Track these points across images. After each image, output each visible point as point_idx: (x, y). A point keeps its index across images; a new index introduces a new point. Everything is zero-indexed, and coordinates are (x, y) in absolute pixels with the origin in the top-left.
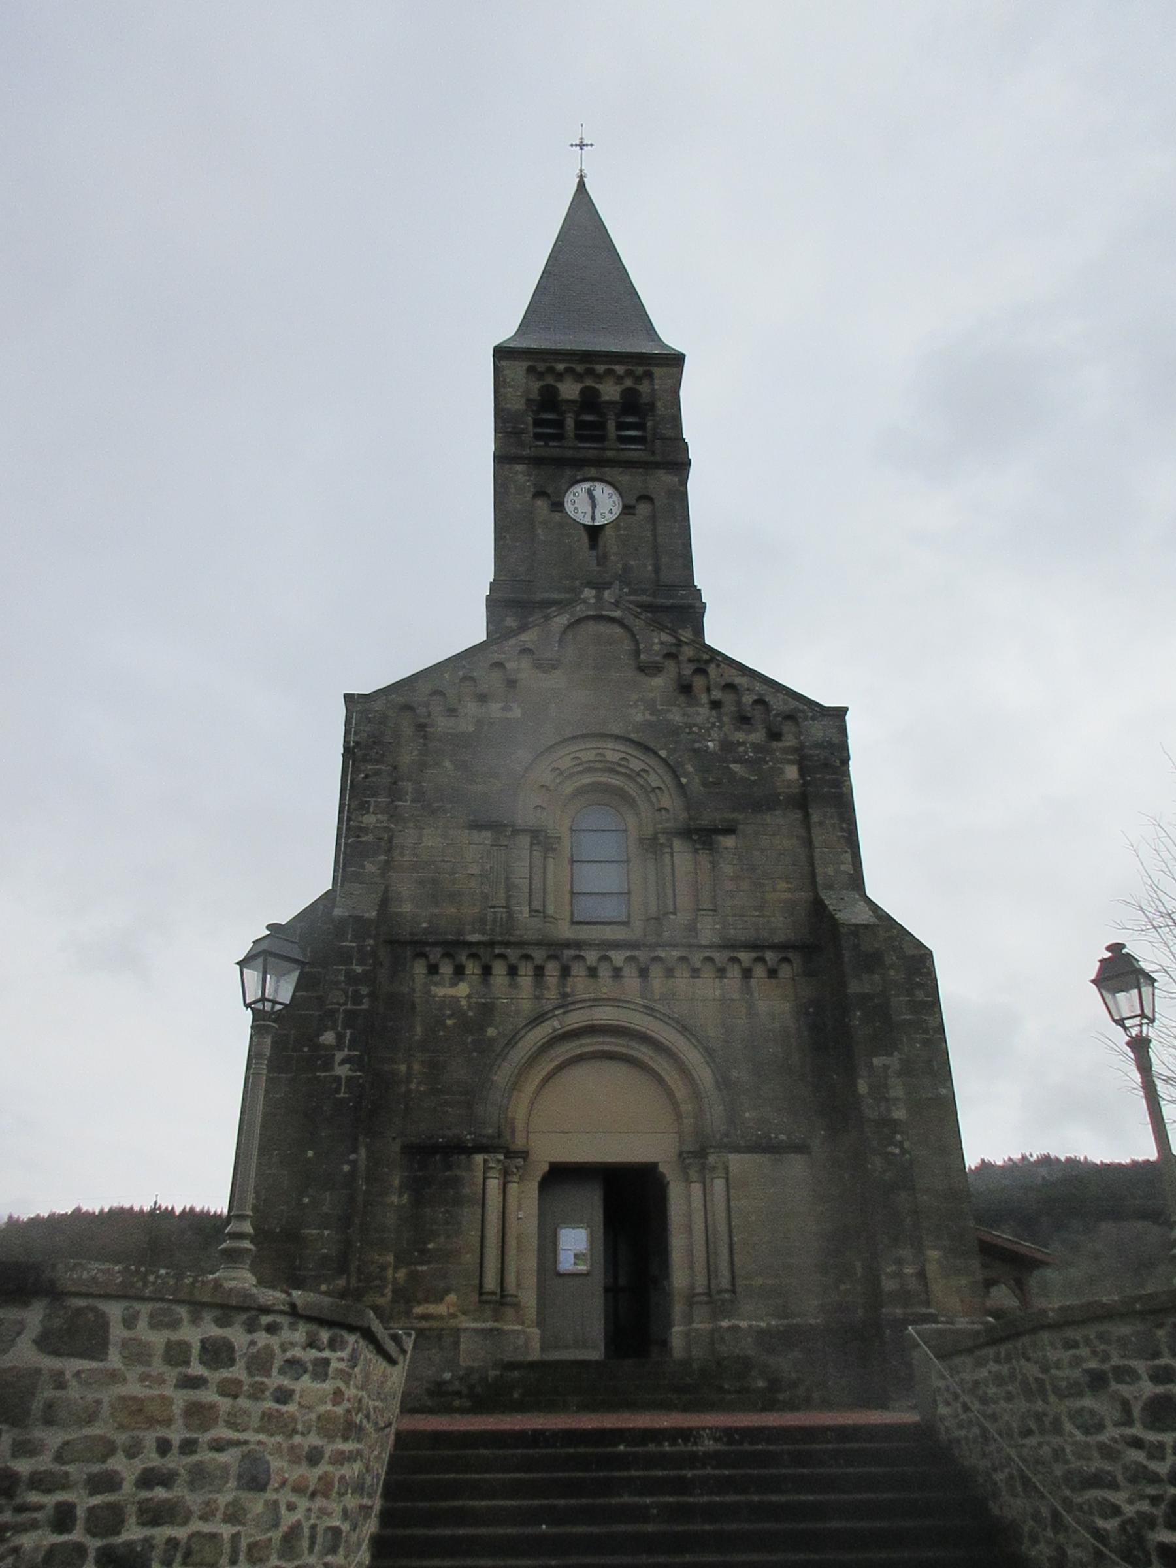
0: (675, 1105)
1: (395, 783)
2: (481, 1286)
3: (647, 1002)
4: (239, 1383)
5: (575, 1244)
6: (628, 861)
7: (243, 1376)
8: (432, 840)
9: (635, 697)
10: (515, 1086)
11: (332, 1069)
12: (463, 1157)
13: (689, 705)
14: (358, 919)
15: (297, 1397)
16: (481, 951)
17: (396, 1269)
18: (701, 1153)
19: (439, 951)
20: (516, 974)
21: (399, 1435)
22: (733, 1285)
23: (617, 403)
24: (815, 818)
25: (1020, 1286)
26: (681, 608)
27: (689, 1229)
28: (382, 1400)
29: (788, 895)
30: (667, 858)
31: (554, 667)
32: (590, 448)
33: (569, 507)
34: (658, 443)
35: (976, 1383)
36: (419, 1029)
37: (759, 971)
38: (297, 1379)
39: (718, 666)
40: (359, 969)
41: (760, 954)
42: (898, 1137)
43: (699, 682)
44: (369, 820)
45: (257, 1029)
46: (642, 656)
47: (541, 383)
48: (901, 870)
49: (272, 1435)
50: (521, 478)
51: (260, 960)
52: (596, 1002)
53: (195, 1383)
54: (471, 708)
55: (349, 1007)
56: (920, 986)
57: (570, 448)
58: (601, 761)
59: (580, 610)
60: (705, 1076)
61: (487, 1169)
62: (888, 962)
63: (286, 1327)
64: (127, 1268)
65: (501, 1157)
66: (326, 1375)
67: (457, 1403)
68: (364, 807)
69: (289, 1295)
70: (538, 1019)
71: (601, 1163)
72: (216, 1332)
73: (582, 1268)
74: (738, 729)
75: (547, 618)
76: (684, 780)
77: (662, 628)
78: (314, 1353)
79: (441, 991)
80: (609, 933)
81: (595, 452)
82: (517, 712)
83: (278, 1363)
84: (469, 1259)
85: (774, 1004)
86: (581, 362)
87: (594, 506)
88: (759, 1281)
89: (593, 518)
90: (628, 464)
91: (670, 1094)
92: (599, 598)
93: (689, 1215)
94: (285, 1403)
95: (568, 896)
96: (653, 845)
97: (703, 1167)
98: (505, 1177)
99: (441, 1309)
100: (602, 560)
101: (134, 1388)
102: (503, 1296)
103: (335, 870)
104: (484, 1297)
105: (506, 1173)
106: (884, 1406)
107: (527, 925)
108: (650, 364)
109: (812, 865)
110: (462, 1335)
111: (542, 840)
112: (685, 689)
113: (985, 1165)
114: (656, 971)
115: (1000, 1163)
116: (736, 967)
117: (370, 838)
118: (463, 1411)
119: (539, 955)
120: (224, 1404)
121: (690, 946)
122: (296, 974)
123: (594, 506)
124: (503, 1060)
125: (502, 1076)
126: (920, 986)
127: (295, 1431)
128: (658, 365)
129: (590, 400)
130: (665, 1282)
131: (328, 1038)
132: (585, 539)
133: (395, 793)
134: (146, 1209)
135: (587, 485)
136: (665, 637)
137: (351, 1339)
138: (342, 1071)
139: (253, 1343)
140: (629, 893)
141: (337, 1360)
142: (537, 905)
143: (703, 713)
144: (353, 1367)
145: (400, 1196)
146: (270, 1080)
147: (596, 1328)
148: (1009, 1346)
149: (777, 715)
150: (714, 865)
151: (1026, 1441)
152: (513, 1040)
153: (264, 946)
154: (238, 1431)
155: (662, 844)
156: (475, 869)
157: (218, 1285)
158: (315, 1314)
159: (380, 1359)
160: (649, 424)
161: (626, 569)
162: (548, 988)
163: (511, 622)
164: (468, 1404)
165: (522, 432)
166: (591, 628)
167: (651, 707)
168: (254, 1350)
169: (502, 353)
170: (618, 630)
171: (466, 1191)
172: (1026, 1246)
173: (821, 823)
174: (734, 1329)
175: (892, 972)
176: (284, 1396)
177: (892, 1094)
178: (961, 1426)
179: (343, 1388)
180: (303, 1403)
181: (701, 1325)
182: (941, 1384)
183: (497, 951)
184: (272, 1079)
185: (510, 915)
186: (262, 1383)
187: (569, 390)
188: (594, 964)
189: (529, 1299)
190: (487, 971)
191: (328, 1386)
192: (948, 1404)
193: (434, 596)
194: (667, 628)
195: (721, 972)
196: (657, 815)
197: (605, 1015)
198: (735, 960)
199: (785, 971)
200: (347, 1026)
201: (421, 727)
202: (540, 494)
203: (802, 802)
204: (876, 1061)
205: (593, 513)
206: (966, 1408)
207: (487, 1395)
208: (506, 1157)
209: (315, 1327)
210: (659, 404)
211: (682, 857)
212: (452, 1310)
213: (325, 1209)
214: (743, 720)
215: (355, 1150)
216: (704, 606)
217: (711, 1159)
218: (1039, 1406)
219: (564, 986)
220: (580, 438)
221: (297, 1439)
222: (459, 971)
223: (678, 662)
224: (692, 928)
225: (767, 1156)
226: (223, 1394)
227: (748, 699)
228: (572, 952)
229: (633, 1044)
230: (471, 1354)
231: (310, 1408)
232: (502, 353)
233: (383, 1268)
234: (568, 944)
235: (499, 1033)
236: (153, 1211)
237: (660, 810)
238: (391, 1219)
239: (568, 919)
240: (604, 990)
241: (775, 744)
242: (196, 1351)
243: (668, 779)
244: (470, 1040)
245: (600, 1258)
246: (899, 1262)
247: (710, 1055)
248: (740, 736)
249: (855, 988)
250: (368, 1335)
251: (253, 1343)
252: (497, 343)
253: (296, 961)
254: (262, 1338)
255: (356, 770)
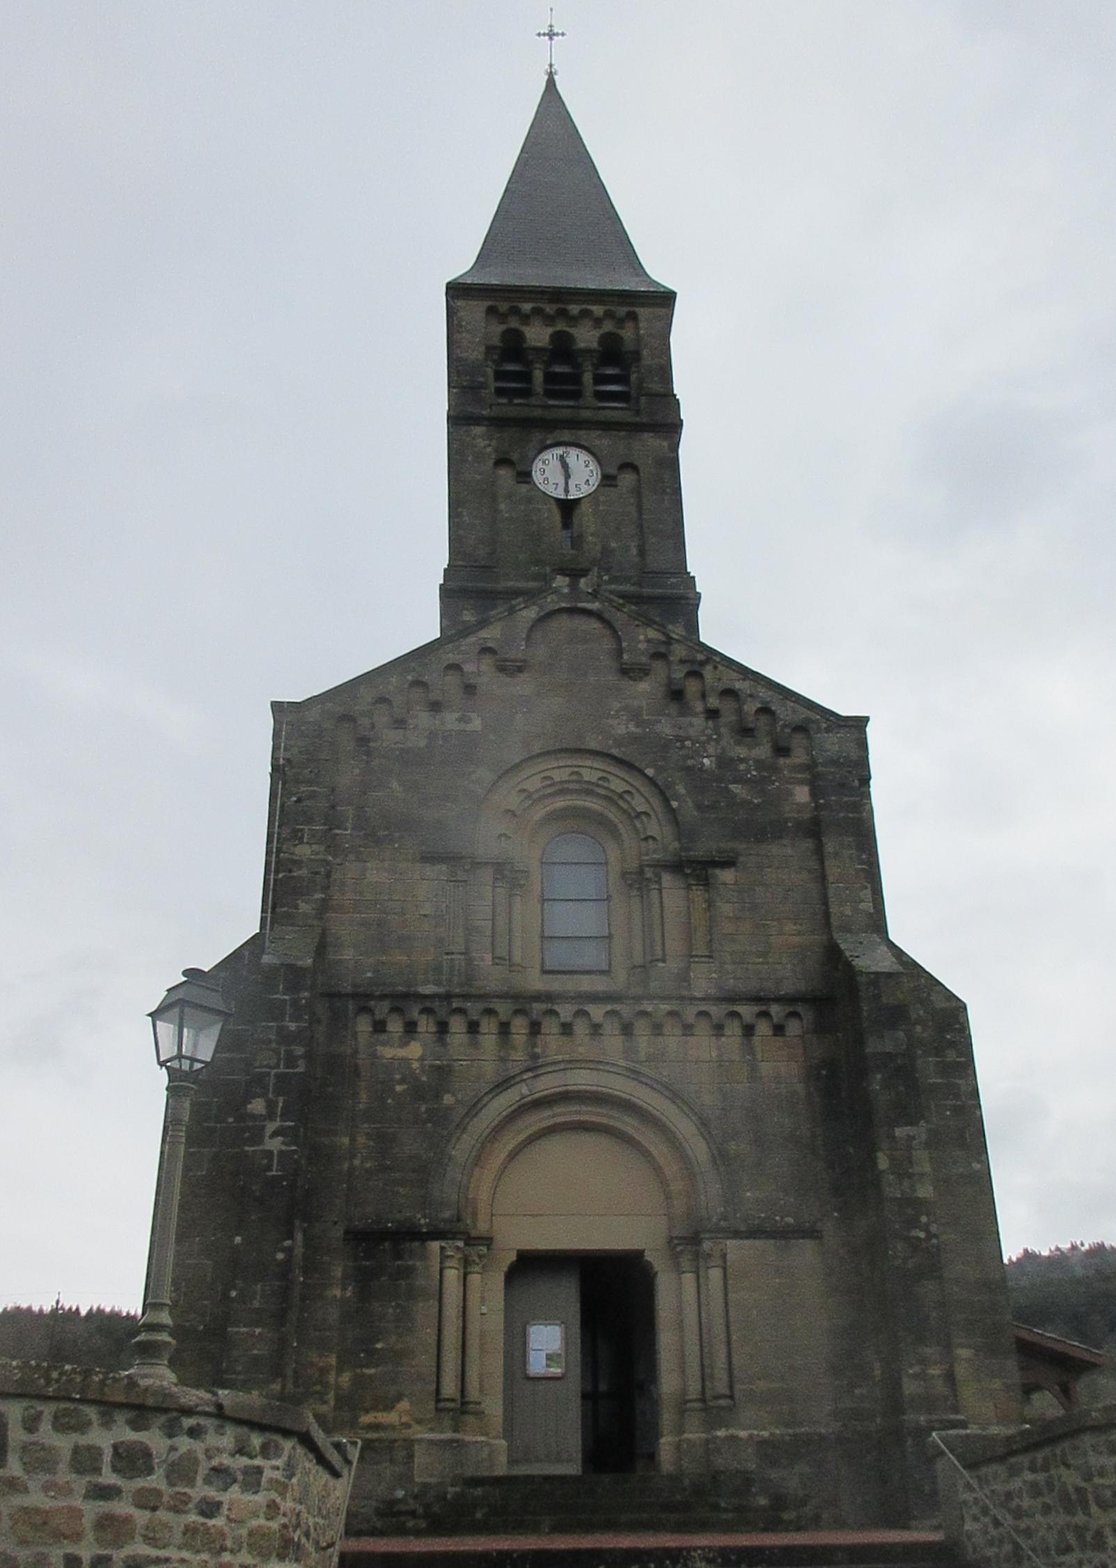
0: (664, 1183)
1: (333, 807)
2: (438, 1391)
3: (631, 1065)
4: (158, 1493)
5: (548, 1343)
6: (609, 899)
7: (163, 1486)
8: (376, 873)
9: (616, 705)
10: (478, 1160)
11: (261, 1142)
12: (417, 1244)
13: (682, 714)
14: (290, 967)
15: (225, 1510)
16: (436, 1004)
17: (340, 1371)
18: (694, 1239)
19: (386, 1005)
20: (478, 1032)
21: (343, 1557)
22: (731, 1387)
23: (595, 351)
24: (830, 847)
25: (1066, 1392)
26: (669, 597)
27: (681, 1325)
28: (323, 1517)
29: (796, 939)
30: (655, 894)
31: (520, 670)
32: (563, 407)
33: (537, 477)
34: (643, 399)
35: (1009, 1495)
36: (364, 1096)
37: (763, 1028)
38: (225, 1490)
39: (715, 668)
40: (293, 1026)
41: (763, 1008)
42: (924, 1219)
43: (692, 687)
44: (303, 851)
45: (173, 1091)
46: (625, 656)
47: (504, 327)
48: (928, 908)
49: (198, 1552)
50: (481, 443)
51: (176, 1010)
52: (573, 1064)
53: (104, 1493)
54: (423, 719)
55: (282, 1070)
56: (952, 1044)
57: (539, 406)
58: (577, 782)
59: (552, 602)
60: (699, 1150)
61: (444, 1258)
62: (914, 1016)
63: (211, 1431)
64: (26, 1364)
65: (461, 1244)
66: (259, 1484)
67: (410, 1524)
68: (297, 837)
69: (215, 1394)
70: (504, 1084)
71: (575, 1251)
72: (130, 1435)
73: (556, 1371)
74: (738, 743)
75: (512, 611)
76: (675, 804)
77: (649, 623)
78: (244, 1461)
79: (388, 1052)
80: (586, 984)
81: (569, 411)
82: (476, 724)
83: (203, 1470)
84: (425, 1361)
85: (781, 1064)
86: (551, 301)
87: (567, 476)
88: (762, 1385)
89: (567, 491)
90: (607, 426)
91: (657, 1170)
92: (573, 586)
93: (680, 1310)
94: (210, 1515)
95: (537, 940)
96: (639, 880)
97: (697, 1256)
98: (465, 1268)
99: (391, 1417)
100: (577, 541)
101: (36, 1499)
102: (464, 1404)
103: (263, 911)
104: (442, 1405)
105: (466, 1262)
106: (905, 1527)
107: (491, 977)
108: (632, 304)
109: (825, 902)
110: (416, 1447)
111: (507, 874)
112: (676, 695)
113: (1028, 1256)
114: (641, 1027)
115: (1045, 1253)
116: (736, 1023)
117: (303, 872)
118: (418, 1533)
119: (504, 1009)
120: (141, 1517)
121: (682, 998)
122: (218, 1027)
123: (567, 476)
124: (462, 1133)
125: (461, 1149)
126: (952, 1044)
127: (223, 1549)
128: (642, 305)
129: (562, 348)
130: (652, 1387)
131: (257, 1106)
132: (557, 517)
133: (333, 821)
134: (47, 1309)
135: (559, 451)
136: (652, 634)
137: (288, 1445)
138: (275, 1145)
139: (173, 1449)
140: (610, 937)
141: (271, 1469)
142: (502, 951)
143: (697, 724)
144: (290, 1477)
145: (344, 1289)
146: (188, 1155)
147: (573, 1442)
148: (1047, 1451)
149: (785, 726)
150: (710, 904)
151: (1063, 1559)
152: (474, 1108)
153: (180, 994)
154: (156, 1547)
155: (648, 880)
156: (427, 909)
157: (132, 1383)
158: (245, 1416)
159: (320, 1468)
160: (633, 377)
161: (607, 552)
162: (515, 1048)
163: (468, 617)
164: (423, 1524)
165: (483, 386)
166: (565, 622)
167: (635, 716)
168: (174, 1456)
169: (456, 291)
170: (595, 625)
171: (420, 1282)
172: (1075, 1346)
173: (836, 854)
174: (733, 1439)
175: (918, 1028)
176: (210, 1509)
177: (917, 1169)
178: (991, 1543)
179: (278, 1500)
180: (232, 1516)
181: (694, 1435)
182: (969, 1497)
183: (455, 1005)
184: (192, 1154)
185: (470, 961)
186: (185, 1494)
187: (538, 335)
188: (569, 1020)
189: (494, 1407)
190: (443, 1028)
191: (260, 1498)
192: (976, 1519)
193: (373, 574)
194: (655, 623)
195: (719, 1029)
196: (643, 844)
197: (581, 1080)
198: (734, 1015)
199: (794, 1028)
200: (278, 1092)
201: (363, 741)
202: (502, 461)
203: (814, 829)
204: (900, 1132)
205: (567, 484)
206: (997, 1524)
207: (446, 1515)
208: (466, 1244)
209: (245, 1429)
210: (645, 353)
211: (673, 895)
212: (404, 1419)
213: (256, 1304)
214: (745, 732)
215: (290, 1236)
216: (698, 597)
217: (707, 1245)
218: (1080, 1519)
219: (534, 1045)
220: (549, 394)
221: (226, 1557)
222: (411, 1028)
223: (669, 663)
224: (684, 977)
225: (772, 1242)
226: (140, 1506)
227: (751, 707)
228: (544, 1006)
229: (615, 1114)
230: (427, 1469)
231: (241, 1522)
232: (456, 291)
233: (324, 1371)
234: (538, 997)
235: (458, 1101)
236: (54, 1311)
237: (646, 839)
238: (334, 1315)
239: (538, 966)
240: (581, 1049)
241: (782, 761)
242: (107, 1456)
243: (656, 802)
244: (423, 1109)
245: (576, 1355)
246: (923, 1361)
247: (703, 1124)
248: (742, 752)
249: (873, 1046)
250: (306, 1440)
251: (173, 1449)
252: (449, 280)
253: (219, 1012)
254: (184, 1444)
255: (287, 793)
